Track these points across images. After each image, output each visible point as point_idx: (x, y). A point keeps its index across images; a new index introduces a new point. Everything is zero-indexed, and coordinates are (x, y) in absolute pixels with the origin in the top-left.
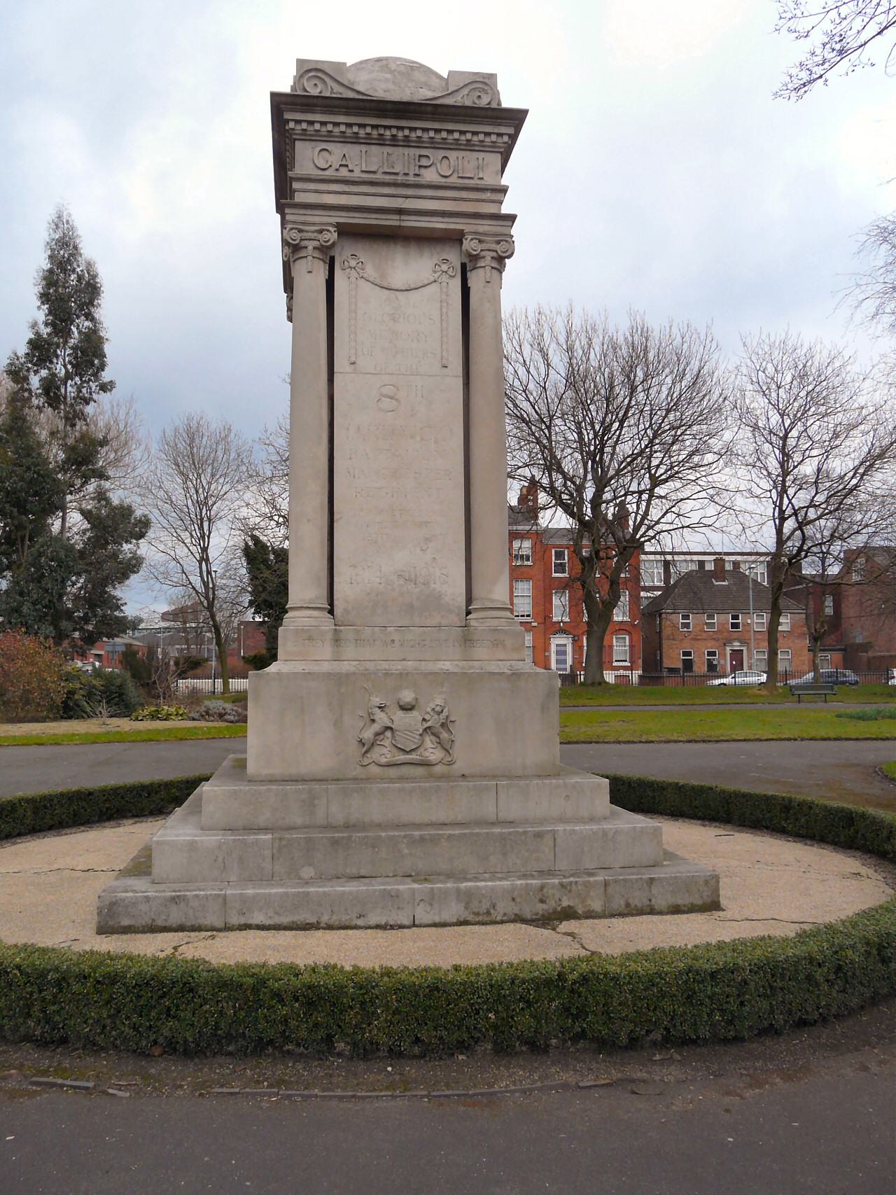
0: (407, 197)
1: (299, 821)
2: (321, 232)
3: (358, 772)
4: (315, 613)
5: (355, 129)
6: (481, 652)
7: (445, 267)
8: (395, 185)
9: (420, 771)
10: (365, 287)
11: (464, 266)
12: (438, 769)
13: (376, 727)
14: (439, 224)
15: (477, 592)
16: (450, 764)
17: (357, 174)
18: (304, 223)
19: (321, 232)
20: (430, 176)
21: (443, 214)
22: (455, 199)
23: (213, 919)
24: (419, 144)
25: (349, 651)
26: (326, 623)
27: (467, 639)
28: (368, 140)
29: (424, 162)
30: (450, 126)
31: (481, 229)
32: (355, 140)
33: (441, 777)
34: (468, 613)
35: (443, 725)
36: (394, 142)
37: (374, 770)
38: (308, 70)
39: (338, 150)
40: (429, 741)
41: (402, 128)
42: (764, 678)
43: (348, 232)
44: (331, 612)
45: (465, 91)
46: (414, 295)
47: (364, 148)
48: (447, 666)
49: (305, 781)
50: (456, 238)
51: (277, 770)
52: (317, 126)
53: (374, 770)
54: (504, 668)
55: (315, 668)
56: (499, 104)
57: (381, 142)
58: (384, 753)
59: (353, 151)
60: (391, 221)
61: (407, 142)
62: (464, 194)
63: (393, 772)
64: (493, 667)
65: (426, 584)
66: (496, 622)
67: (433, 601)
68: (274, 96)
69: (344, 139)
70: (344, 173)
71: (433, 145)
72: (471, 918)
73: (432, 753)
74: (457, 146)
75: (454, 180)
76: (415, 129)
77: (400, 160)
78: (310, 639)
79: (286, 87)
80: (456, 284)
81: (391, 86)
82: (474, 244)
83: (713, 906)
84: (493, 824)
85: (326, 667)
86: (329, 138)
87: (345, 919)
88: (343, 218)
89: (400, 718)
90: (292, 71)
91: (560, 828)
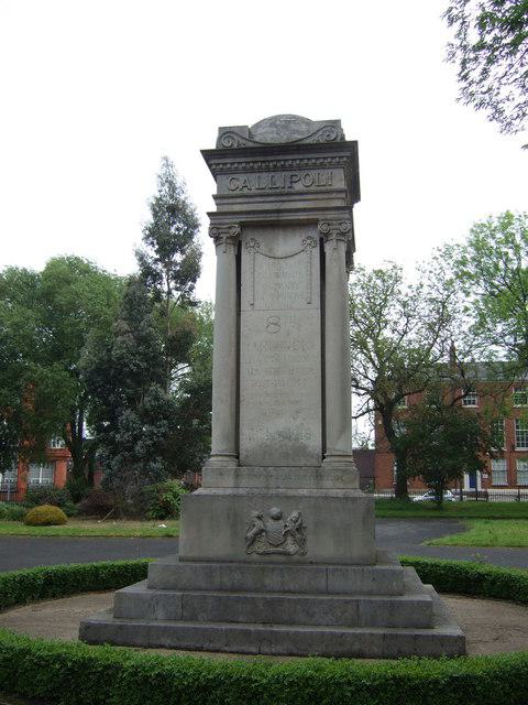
0: (232, 204)
1: (204, 585)
2: (230, 228)
3: (245, 557)
4: (226, 459)
5: (251, 165)
6: (328, 483)
7: (309, 242)
8: (277, 195)
9: (282, 558)
10: (260, 258)
11: (321, 239)
12: (296, 557)
13: (255, 530)
14: (303, 216)
15: (328, 445)
16: (303, 554)
17: (254, 191)
18: (220, 224)
19: (230, 228)
20: (298, 187)
21: (304, 210)
22: (271, 202)
23: (139, 640)
24: (291, 168)
25: (244, 482)
26: (232, 465)
27: (319, 475)
28: (260, 170)
29: (295, 179)
30: (309, 156)
31: (329, 217)
32: (252, 171)
33: (298, 562)
34: (324, 458)
35: (297, 530)
36: (276, 169)
37: (255, 556)
38: (225, 133)
39: (242, 177)
40: (290, 540)
41: (280, 161)
42: (388, 494)
43: (243, 226)
44: (238, 457)
45: (321, 133)
46: (290, 261)
47: (257, 175)
48: (305, 492)
49: (224, 562)
50: (313, 223)
51: (195, 554)
52: (229, 166)
53: (255, 556)
54: (340, 493)
55: (220, 492)
56: (343, 137)
57: (268, 170)
58: (261, 547)
59: (253, 177)
60: (273, 217)
61: (284, 169)
62: (320, 196)
63: (267, 558)
64: (333, 493)
65: (297, 439)
66: (335, 464)
67: (301, 450)
68: (208, 155)
69: (245, 171)
70: (246, 191)
71: (300, 168)
72: (295, 651)
73: (291, 547)
74: (315, 167)
75: (313, 188)
76: (295, 160)
77: (280, 179)
78: (221, 474)
79: (212, 146)
80: (316, 252)
81: (275, 135)
82: (324, 227)
83: (462, 653)
84: (322, 593)
85: (229, 492)
86: (236, 171)
87: (218, 646)
88: (243, 219)
89: (271, 525)
90: (215, 135)
91: (362, 598)
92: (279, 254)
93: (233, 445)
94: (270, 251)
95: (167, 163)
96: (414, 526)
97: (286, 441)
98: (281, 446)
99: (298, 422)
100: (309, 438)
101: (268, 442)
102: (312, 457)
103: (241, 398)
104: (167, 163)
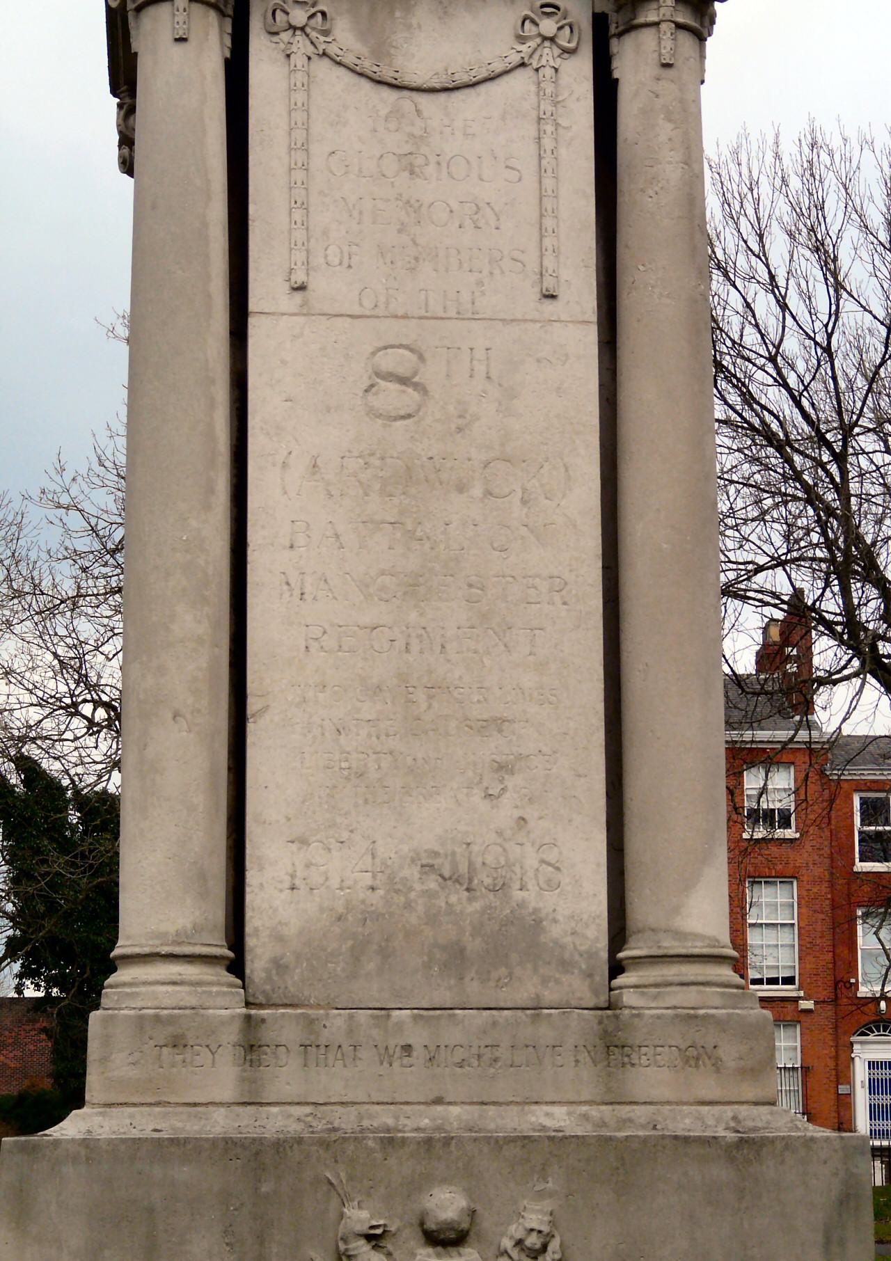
34: (616, 969)
44: (237, 967)
48: (558, 1118)
64: (686, 1122)
65: (500, 888)
66: (688, 997)
78: (177, 1043)
80: (580, 71)
85: (220, 1123)
92: (418, 69)
93: (217, 913)
94: (381, 51)
95: (812, 121)
96: (565, 1108)
97: (457, 897)
98: (432, 919)
99: (505, 814)
100: (552, 885)
101: (376, 898)
102: (565, 965)
103: (253, 705)
104: (812, 121)
